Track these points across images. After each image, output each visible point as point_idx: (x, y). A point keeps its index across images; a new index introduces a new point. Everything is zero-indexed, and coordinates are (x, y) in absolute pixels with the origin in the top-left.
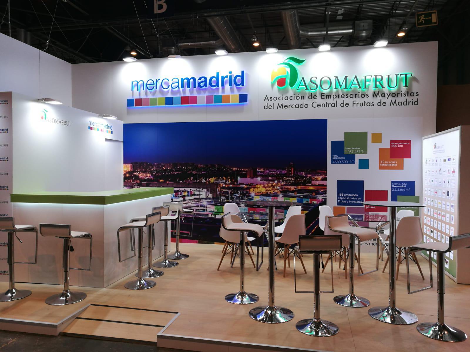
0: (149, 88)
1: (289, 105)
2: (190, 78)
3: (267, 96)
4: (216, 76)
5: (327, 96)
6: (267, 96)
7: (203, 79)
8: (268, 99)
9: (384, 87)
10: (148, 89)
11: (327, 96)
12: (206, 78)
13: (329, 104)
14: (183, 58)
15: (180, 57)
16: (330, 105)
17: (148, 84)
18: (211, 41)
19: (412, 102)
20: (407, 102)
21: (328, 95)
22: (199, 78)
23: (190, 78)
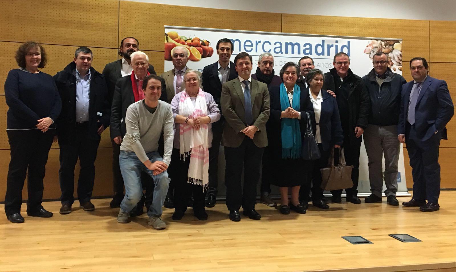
0: (302, 60)
1: (257, 43)
2: (294, 43)
3: (318, 63)
4: (321, 43)
5: (290, 47)
6: (318, 63)
7: (308, 47)
8: (319, 66)
9: (155, 107)
10: (301, 60)
11: (290, 47)
12: (281, 44)
13: (257, 43)
14: (71, 219)
15: (140, 200)
16: (259, 44)
17: (280, 48)
18: (346, 161)
19: (337, 46)
20: (323, 46)
21: (291, 43)
22: (304, 45)
23: (294, 43)
